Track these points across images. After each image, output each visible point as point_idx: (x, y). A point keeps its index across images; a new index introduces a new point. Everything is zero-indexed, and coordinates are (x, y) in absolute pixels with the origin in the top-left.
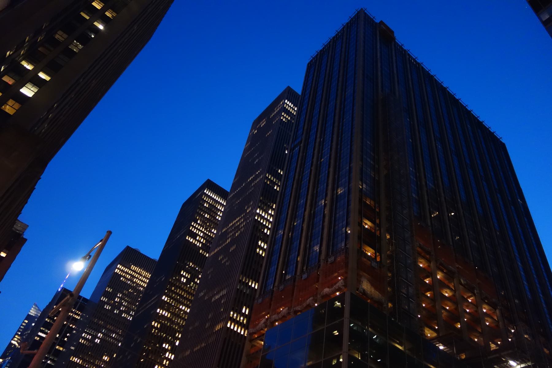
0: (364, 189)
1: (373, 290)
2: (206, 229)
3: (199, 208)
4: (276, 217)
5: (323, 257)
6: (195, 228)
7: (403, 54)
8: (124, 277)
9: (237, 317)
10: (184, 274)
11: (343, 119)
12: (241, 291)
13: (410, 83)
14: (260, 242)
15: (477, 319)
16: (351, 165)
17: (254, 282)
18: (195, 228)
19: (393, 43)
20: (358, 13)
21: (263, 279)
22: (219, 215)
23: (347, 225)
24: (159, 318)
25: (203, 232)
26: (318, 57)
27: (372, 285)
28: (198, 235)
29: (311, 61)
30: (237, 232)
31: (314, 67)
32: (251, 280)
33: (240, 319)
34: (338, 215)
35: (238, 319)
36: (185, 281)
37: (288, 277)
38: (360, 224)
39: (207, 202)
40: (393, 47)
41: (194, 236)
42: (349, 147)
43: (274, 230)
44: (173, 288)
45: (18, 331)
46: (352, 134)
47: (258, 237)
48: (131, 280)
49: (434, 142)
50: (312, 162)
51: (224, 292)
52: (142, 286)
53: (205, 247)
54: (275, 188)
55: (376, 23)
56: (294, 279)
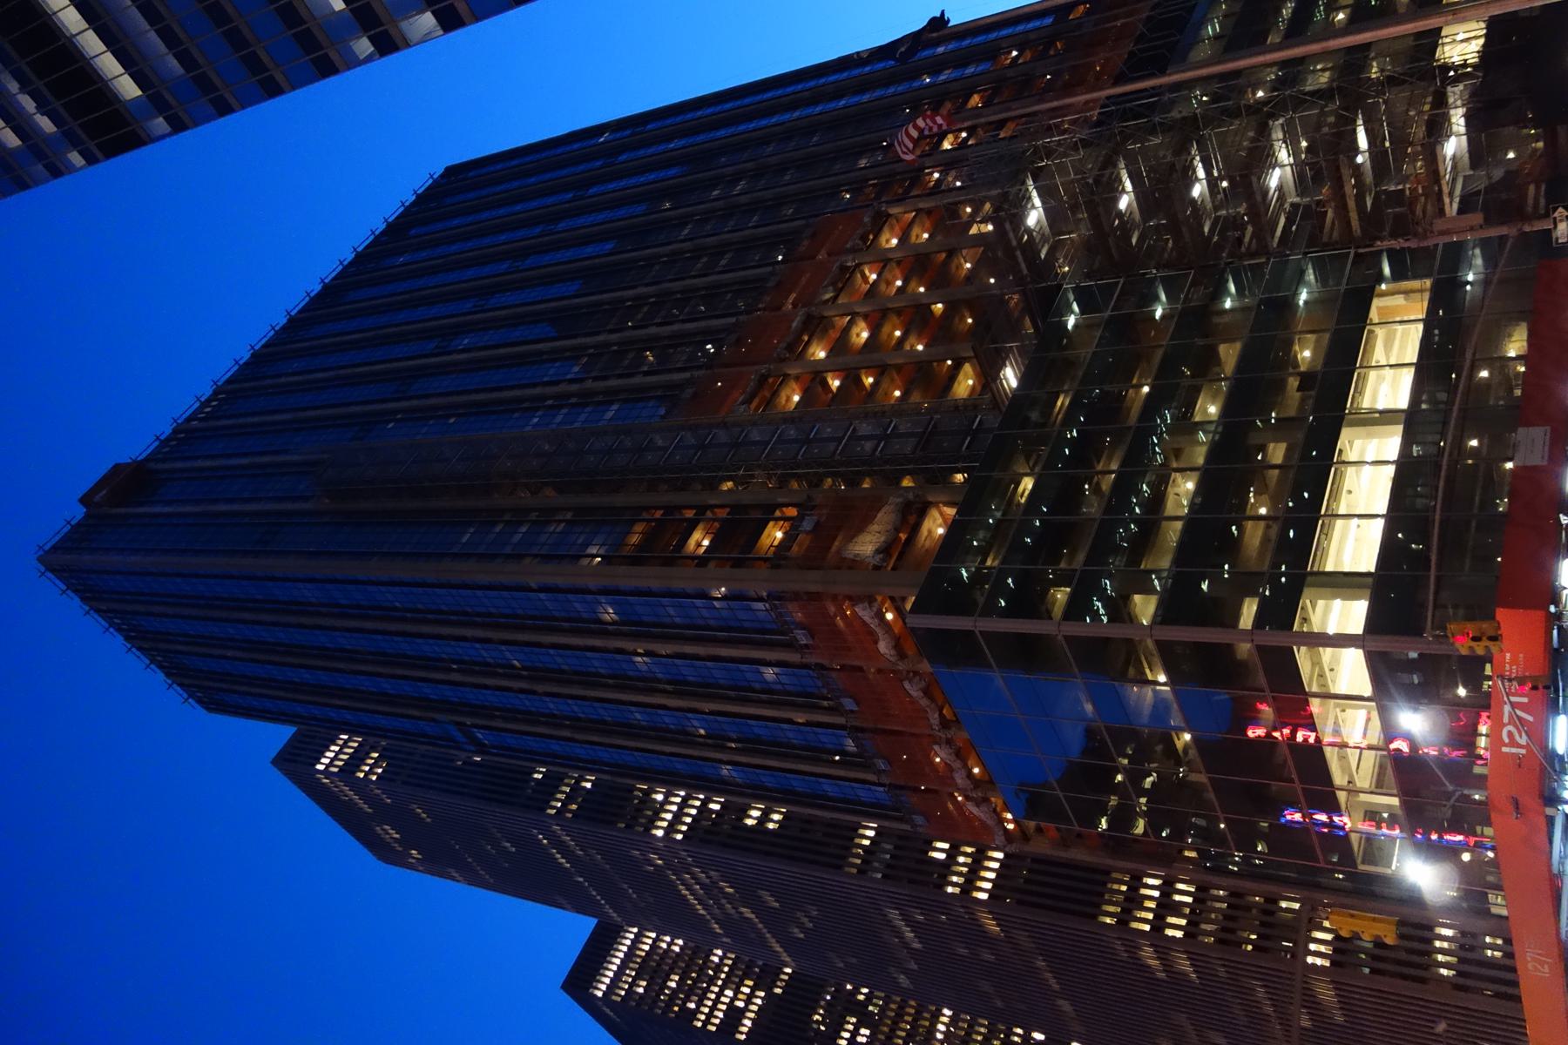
0: (602, 552)
1: (875, 527)
2: (712, 981)
3: (651, 1009)
4: (672, 783)
5: (794, 657)
7: (186, 437)
9: (960, 874)
11: (396, 609)
12: (888, 866)
13: (277, 417)
14: (750, 822)
15: (916, 263)
16: (533, 585)
17: (861, 831)
18: (710, 1015)
19: (152, 465)
20: (53, 571)
21: (848, 812)
22: (669, 944)
23: (705, 596)
26: (187, 682)
27: (861, 528)
28: (731, 1005)
29: (200, 701)
31: (217, 690)
32: (857, 841)
33: (964, 865)
34: (677, 620)
35: (965, 870)
36: (867, 1032)
37: (850, 745)
38: (702, 561)
40: (167, 466)
41: (735, 1015)
42: (479, 593)
43: (713, 786)
46: (441, 586)
47: (734, 828)
49: (455, 357)
50: (522, 691)
51: (894, 914)
53: (765, 980)
54: (588, 785)
55: (87, 516)
56: (854, 732)
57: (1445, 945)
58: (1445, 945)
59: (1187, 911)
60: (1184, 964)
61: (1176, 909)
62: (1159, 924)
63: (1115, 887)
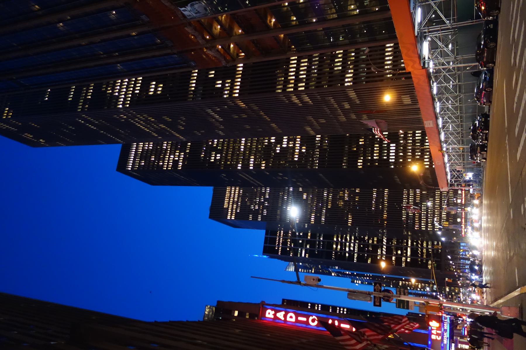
2: (165, 154)
6: (168, 165)
8: (236, 210)
9: (227, 90)
10: (213, 158)
14: (151, 93)
17: (191, 85)
18: (168, 165)
24: (257, 166)
25: (169, 156)
28: (174, 160)
30: (150, 120)
32: (190, 89)
36: (219, 155)
39: (140, 163)
41: (176, 163)
44: (229, 163)
45: (309, 272)
48: (238, 202)
51: (209, 111)
52: (239, 192)
53: (183, 149)
57: (389, 67)
58: (389, 67)
59: (305, 80)
60: (307, 99)
61: (301, 81)
62: (296, 87)
63: (280, 79)
